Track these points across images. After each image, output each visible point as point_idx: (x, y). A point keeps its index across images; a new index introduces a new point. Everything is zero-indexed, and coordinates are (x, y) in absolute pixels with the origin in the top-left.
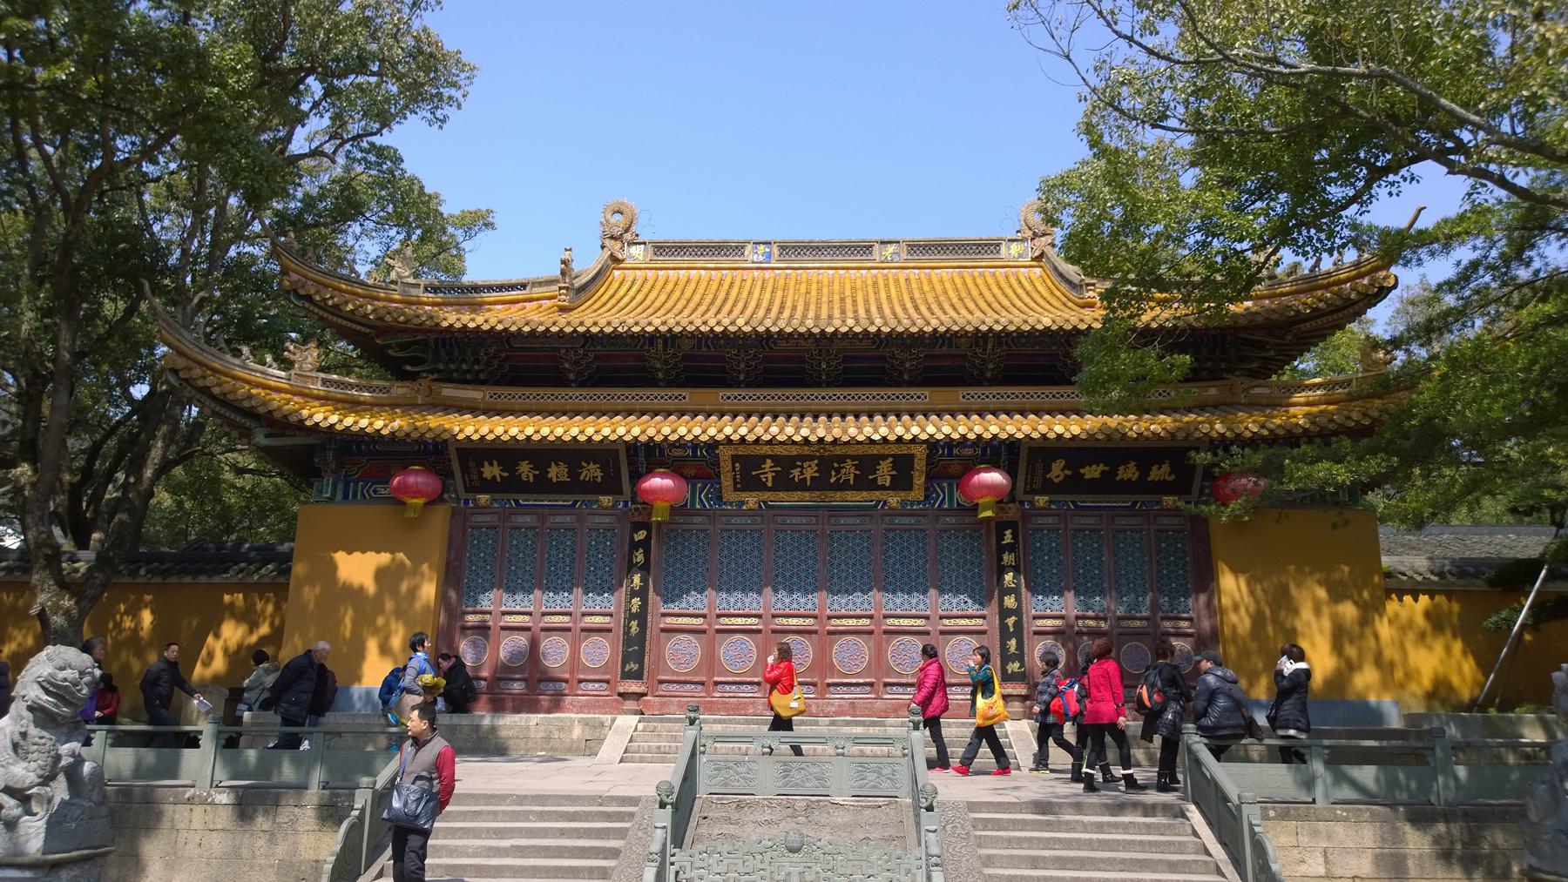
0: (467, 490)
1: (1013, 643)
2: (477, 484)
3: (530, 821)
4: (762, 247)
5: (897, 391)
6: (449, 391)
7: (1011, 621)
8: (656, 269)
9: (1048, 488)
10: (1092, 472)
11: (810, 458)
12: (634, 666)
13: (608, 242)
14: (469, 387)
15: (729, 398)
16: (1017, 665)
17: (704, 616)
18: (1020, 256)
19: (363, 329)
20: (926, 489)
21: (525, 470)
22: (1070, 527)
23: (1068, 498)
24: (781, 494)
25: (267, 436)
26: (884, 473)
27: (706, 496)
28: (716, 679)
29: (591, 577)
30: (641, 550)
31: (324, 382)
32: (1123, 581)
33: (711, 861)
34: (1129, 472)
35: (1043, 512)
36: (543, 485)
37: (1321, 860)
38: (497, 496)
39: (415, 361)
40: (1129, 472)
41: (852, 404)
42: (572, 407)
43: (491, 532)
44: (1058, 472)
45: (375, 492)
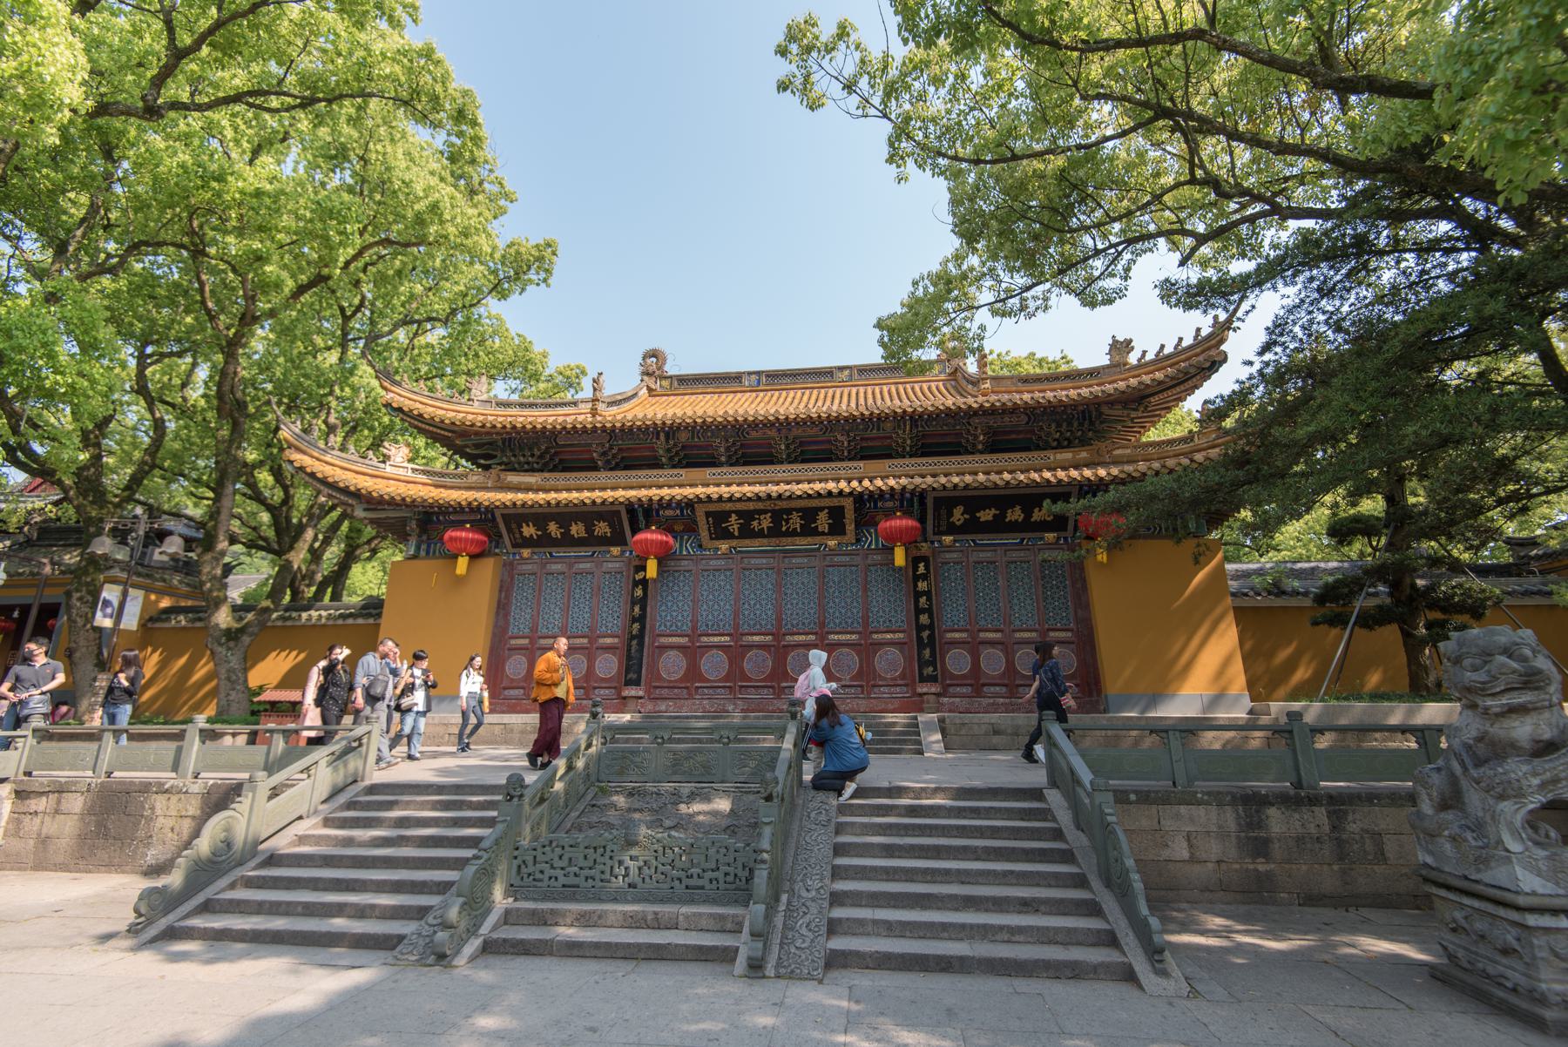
0: (515, 546)
1: (927, 652)
2: (520, 541)
5: (839, 464)
7: (925, 634)
9: (952, 529)
10: (986, 515)
11: (765, 512)
12: (632, 676)
13: (645, 378)
16: (931, 669)
21: (553, 528)
22: (971, 560)
23: (969, 537)
25: (365, 510)
26: (823, 521)
31: (414, 470)
32: (1016, 601)
34: (1015, 514)
35: (949, 549)
36: (567, 541)
37: (1185, 844)
38: (536, 550)
39: (487, 457)
40: (1015, 514)
43: (532, 577)
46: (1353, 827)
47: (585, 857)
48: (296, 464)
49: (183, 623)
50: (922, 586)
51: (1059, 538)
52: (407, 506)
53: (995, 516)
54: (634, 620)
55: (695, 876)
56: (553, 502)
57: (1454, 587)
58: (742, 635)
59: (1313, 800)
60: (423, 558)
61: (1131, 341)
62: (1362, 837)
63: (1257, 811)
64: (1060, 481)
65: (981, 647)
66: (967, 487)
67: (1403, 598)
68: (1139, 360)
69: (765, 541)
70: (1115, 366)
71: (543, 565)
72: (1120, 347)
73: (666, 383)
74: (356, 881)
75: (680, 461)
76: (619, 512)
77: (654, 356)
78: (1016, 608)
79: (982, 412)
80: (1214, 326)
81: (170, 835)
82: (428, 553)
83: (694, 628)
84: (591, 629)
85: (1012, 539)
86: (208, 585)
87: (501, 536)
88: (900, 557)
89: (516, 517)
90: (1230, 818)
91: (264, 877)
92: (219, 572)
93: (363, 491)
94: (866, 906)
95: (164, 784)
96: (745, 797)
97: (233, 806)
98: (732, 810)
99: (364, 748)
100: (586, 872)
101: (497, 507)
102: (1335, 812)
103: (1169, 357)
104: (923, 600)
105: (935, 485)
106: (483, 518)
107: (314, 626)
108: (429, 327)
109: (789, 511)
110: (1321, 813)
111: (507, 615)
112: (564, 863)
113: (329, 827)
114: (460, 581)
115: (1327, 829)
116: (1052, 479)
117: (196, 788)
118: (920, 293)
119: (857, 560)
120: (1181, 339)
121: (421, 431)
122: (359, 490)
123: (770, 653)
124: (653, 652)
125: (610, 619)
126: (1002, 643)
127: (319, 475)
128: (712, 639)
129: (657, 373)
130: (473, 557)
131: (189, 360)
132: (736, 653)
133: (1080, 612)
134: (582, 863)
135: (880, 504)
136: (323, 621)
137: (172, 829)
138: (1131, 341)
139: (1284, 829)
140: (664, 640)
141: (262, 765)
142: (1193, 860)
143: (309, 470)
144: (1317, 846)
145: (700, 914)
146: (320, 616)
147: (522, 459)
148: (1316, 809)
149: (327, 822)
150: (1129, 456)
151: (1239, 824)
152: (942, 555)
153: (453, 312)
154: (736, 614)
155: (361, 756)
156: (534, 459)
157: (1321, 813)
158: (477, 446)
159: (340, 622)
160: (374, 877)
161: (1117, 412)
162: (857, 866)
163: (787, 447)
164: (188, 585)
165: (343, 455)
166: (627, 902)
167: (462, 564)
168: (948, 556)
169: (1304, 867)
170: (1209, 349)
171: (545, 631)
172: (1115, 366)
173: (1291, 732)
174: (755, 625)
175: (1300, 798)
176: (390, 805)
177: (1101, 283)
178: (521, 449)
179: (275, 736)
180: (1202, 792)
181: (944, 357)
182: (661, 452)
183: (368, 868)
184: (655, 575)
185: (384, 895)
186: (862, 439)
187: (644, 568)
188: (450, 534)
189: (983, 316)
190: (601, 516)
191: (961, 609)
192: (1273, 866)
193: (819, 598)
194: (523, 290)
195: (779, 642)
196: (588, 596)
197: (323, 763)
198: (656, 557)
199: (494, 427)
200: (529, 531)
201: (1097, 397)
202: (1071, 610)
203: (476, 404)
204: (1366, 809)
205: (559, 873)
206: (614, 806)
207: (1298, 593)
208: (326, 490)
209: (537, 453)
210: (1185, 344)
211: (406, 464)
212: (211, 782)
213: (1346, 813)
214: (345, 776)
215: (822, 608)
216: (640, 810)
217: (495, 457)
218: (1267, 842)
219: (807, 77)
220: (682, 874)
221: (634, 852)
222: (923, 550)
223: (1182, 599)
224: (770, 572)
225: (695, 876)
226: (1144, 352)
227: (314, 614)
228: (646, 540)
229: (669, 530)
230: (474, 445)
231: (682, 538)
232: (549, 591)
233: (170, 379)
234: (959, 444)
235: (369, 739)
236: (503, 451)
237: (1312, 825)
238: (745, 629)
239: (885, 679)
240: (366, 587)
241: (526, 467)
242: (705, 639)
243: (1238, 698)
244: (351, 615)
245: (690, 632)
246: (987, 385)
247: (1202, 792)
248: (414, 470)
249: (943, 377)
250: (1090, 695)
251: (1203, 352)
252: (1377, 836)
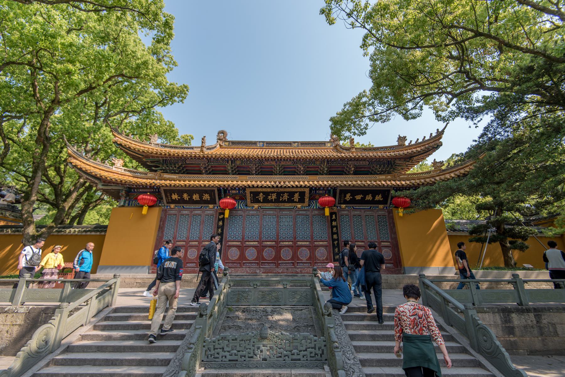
0: (168, 203)
2: (170, 201)
7: (336, 242)
9: (345, 202)
10: (358, 197)
11: (274, 192)
13: (219, 141)
21: (185, 196)
22: (352, 214)
23: (351, 205)
25: (103, 185)
26: (296, 197)
31: (125, 170)
35: (344, 210)
36: (191, 201)
38: (177, 205)
40: (369, 197)
43: (174, 216)
46: (545, 321)
48: (73, 164)
49: (10, 232)
50: (334, 223)
51: (384, 207)
52: (122, 184)
53: (362, 198)
55: (296, 354)
56: (188, 185)
57: (520, 229)
58: (263, 241)
59: (528, 311)
60: (127, 207)
61: (406, 137)
62: (548, 326)
63: (508, 315)
64: (388, 185)
65: (382, 248)
66: (354, 186)
67: (501, 233)
68: (409, 144)
69: (273, 204)
70: (400, 146)
71: (180, 211)
72: (402, 139)
73: (227, 143)
74: (117, 360)
75: (236, 172)
76: (214, 190)
77: (222, 133)
78: (369, 233)
79: (351, 159)
80: (437, 133)
81: (6, 334)
82: (129, 205)
83: (243, 238)
84: (200, 238)
85: (367, 207)
86: (26, 215)
87: (162, 199)
88: (327, 212)
89: (169, 191)
91: (65, 359)
92: (31, 210)
93: (103, 177)
94: (375, 366)
95: (4, 308)
96: (296, 312)
97: (50, 321)
98: (293, 319)
99: (113, 289)
101: (163, 186)
102: (537, 315)
103: (420, 143)
104: (335, 229)
105: (342, 185)
106: (155, 191)
107: (72, 235)
108: (131, 115)
109: (284, 193)
110: (532, 315)
111: (163, 232)
113: (96, 330)
114: (143, 216)
115: (535, 322)
116: (385, 184)
117: (23, 310)
118: (346, 110)
119: (308, 213)
120: (425, 137)
121: (128, 154)
122: (101, 176)
123: (274, 249)
124: (226, 248)
125: (208, 234)
127: (84, 169)
128: (250, 243)
129: (224, 139)
130: (150, 207)
131: (22, 121)
132: (260, 249)
133: (393, 236)
134: (238, 349)
136: (76, 233)
137: (7, 332)
138: (406, 137)
139: (519, 323)
140: (230, 243)
141: (59, 298)
143: (79, 167)
144: (532, 329)
145: (302, 374)
146: (75, 231)
147: (171, 168)
148: (530, 314)
149: (95, 327)
150: (406, 178)
151: (502, 321)
152: (341, 212)
153: (142, 110)
154: (260, 233)
155: (111, 294)
157: (532, 315)
158: (152, 162)
159: (84, 234)
160: (127, 358)
161: (397, 161)
162: (364, 346)
164: (13, 216)
165: (95, 162)
166: (262, 368)
167: (145, 210)
168: (343, 212)
169: (528, 339)
170: (436, 141)
171: (179, 238)
172: (400, 146)
173: (516, 282)
174: (268, 238)
175: (522, 310)
176: (127, 318)
177: (411, 111)
178: (171, 164)
179: (67, 284)
180: (486, 308)
181: (332, 140)
182: (229, 168)
183: (121, 352)
184: (227, 217)
185: (133, 367)
186: (307, 167)
187: (224, 214)
188: (141, 197)
189: (366, 120)
190: (206, 192)
191: (348, 233)
192: (516, 338)
193: (294, 227)
194: (172, 103)
195: (295, 245)
196: (198, 224)
197: (94, 298)
198: (229, 209)
199: (161, 154)
200: (175, 197)
201: (397, 156)
202: (389, 234)
203: (153, 145)
204: (548, 314)
206: (238, 317)
207: (461, 231)
208: (85, 176)
209: (177, 166)
210: (426, 139)
211: (121, 167)
212: (31, 307)
213: (541, 315)
214: (104, 304)
215: (295, 231)
216: (251, 319)
217: (159, 167)
218: (513, 328)
219: (330, 10)
220: (288, 353)
221: (265, 342)
222: (335, 210)
223: (430, 231)
224: (274, 216)
226: (411, 141)
227: (72, 230)
228: (228, 202)
229: (234, 198)
230: (151, 161)
231: (239, 202)
232: (182, 222)
233: (12, 129)
234: (343, 171)
235: (115, 285)
236: (163, 165)
237: (529, 321)
238: (264, 239)
239: (320, 260)
240: (90, 221)
241: (172, 171)
242: (247, 243)
243: (451, 269)
244: (89, 231)
245: (241, 240)
246: (354, 150)
247: (486, 308)
248: (125, 170)
249: (332, 148)
250: (398, 267)
251: (434, 142)
252: (554, 325)
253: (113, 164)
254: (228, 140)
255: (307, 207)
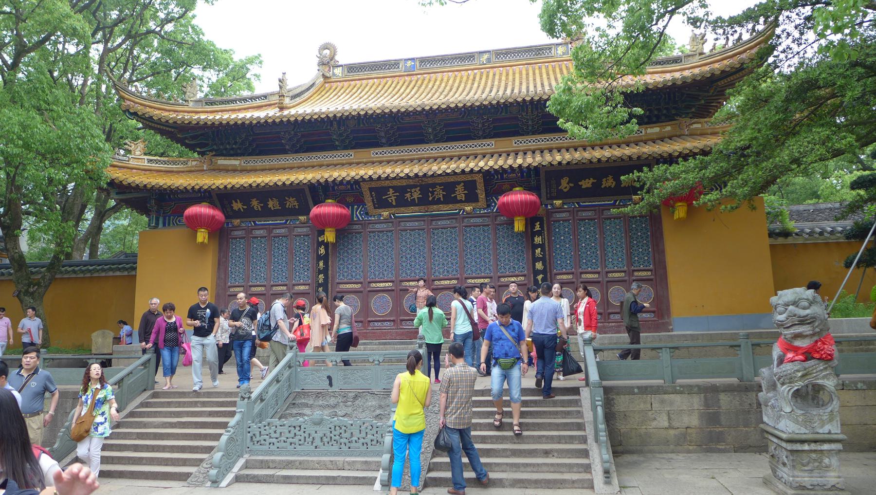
3: (198, 407)
4: (410, 62)
6: (222, 162)
8: (349, 81)
9: (560, 195)
10: (586, 184)
11: (415, 186)
14: (232, 158)
15: (377, 154)
17: (361, 283)
18: (564, 54)
19: (170, 129)
20: (487, 201)
21: (255, 203)
24: (402, 209)
25: (117, 194)
26: (460, 192)
27: (360, 213)
28: (369, 319)
29: (298, 264)
30: (323, 247)
31: (150, 161)
33: (270, 431)
34: (608, 182)
35: (560, 210)
36: (267, 213)
37: (666, 418)
38: (243, 220)
39: (201, 145)
41: (386, 157)
42: (289, 166)
44: (566, 185)
45: (179, 221)
47: (290, 432)
53: (593, 184)
54: (320, 272)
69: (417, 208)
78: (610, 255)
90: (697, 402)
100: (291, 440)
104: (538, 251)
112: (277, 435)
126: (599, 282)
128: (378, 285)
134: (288, 435)
135: (505, 176)
142: (670, 427)
156: (237, 146)
163: (434, 129)
205: (274, 440)
225: (354, 442)
248: (150, 161)
253: (128, 151)
254: (340, 63)
255: (484, 209)
